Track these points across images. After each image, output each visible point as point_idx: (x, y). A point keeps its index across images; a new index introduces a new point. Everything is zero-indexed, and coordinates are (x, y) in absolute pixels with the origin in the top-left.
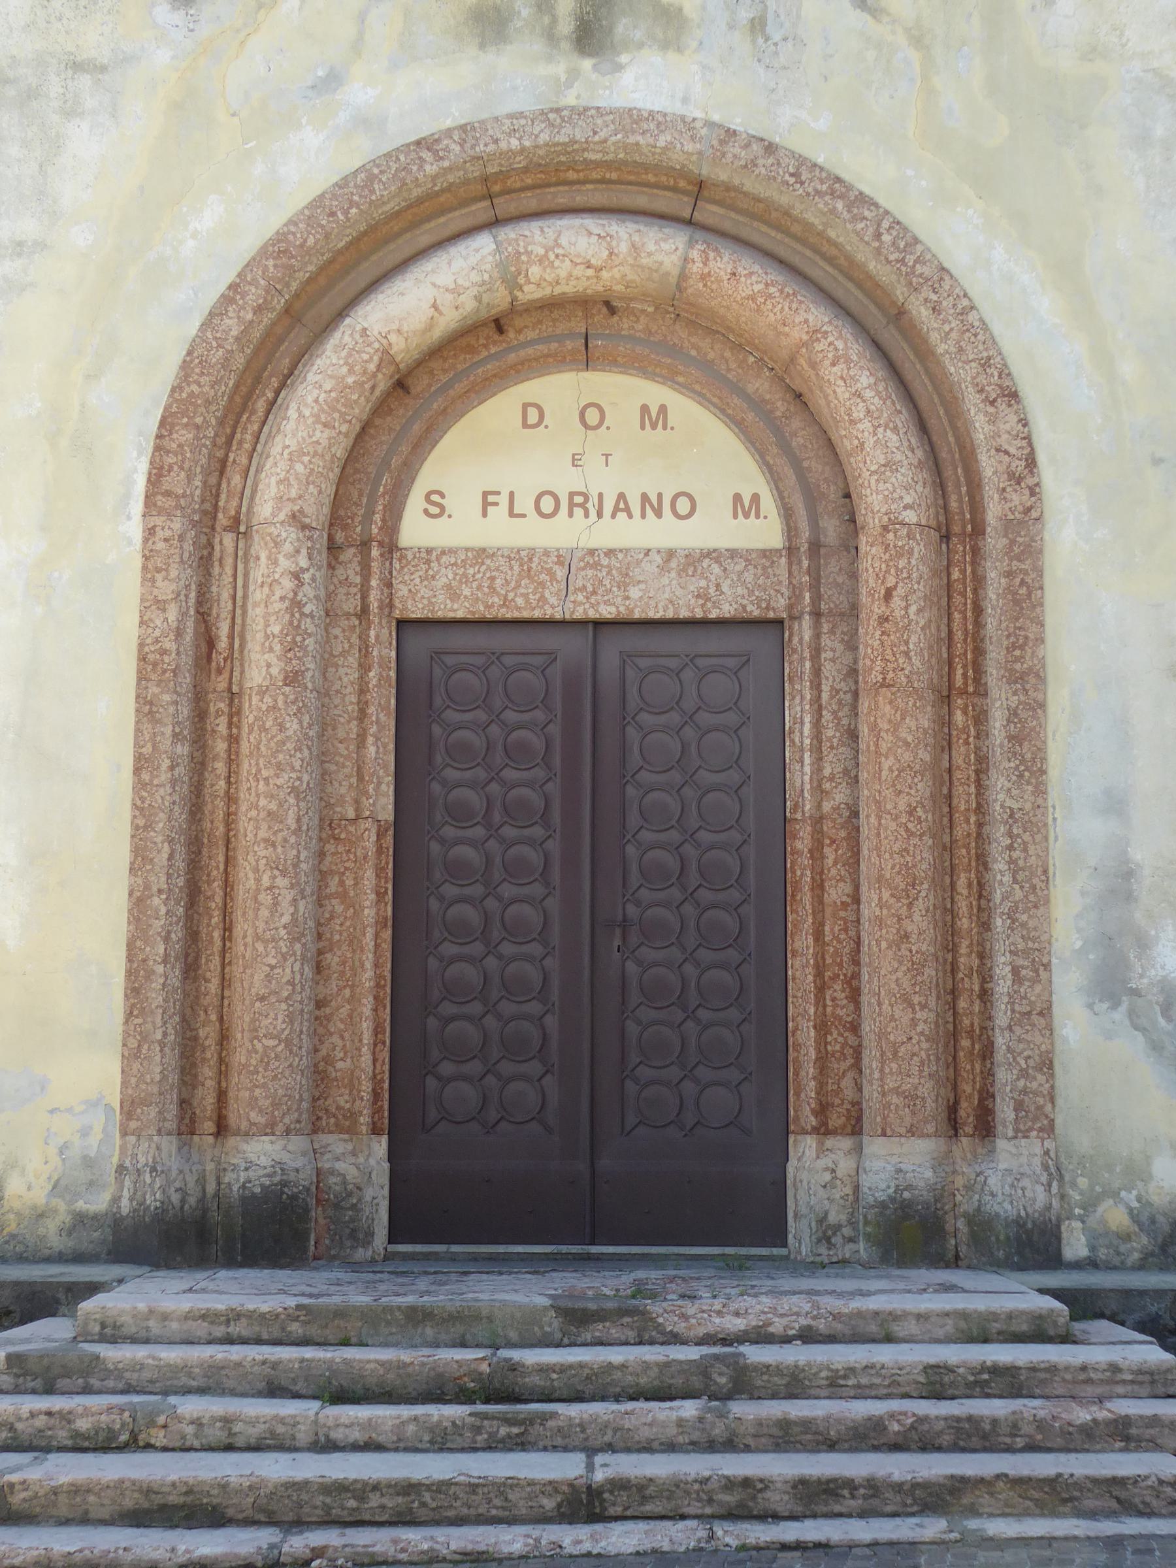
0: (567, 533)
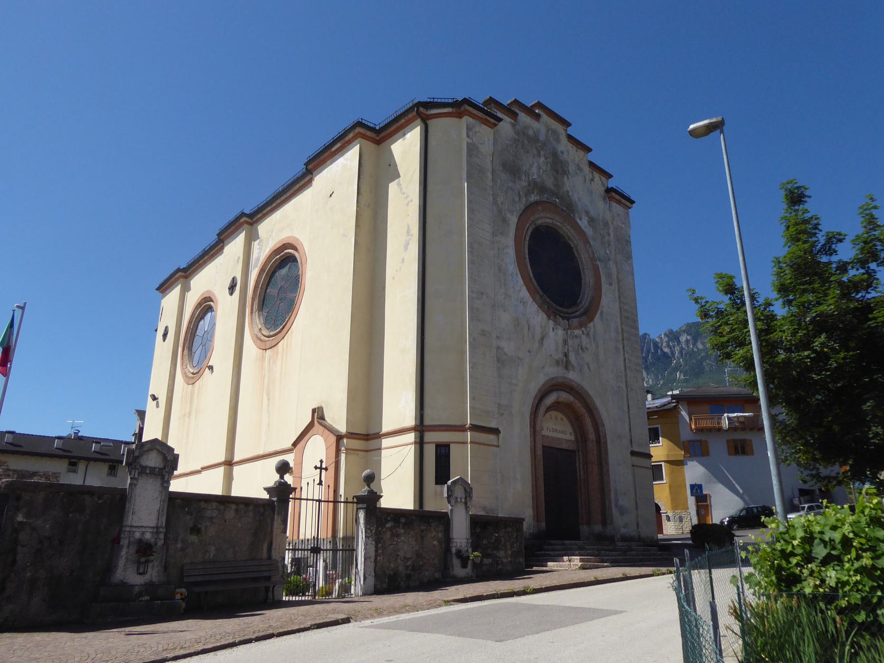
0: (554, 435)
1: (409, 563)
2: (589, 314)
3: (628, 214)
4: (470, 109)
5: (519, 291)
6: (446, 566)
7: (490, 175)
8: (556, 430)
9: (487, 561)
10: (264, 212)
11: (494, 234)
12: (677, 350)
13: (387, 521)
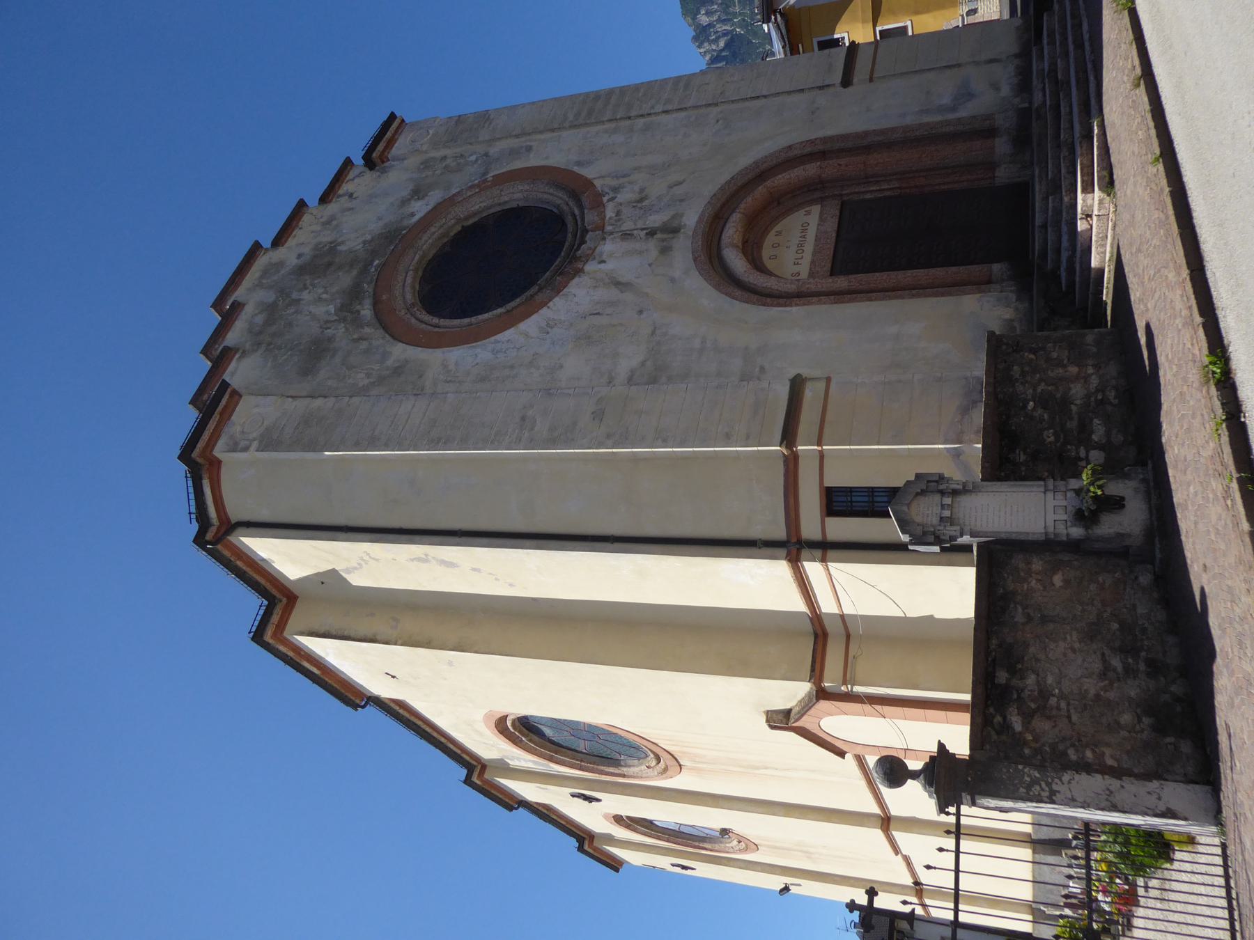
0: (809, 249)
1: (1116, 662)
2: (577, 188)
3: (412, 124)
4: (200, 445)
5: (527, 336)
6: (1119, 554)
7: (319, 402)
8: (801, 245)
9: (1099, 431)
10: (459, 752)
11: (418, 393)
12: (721, 28)
13: (1006, 727)
